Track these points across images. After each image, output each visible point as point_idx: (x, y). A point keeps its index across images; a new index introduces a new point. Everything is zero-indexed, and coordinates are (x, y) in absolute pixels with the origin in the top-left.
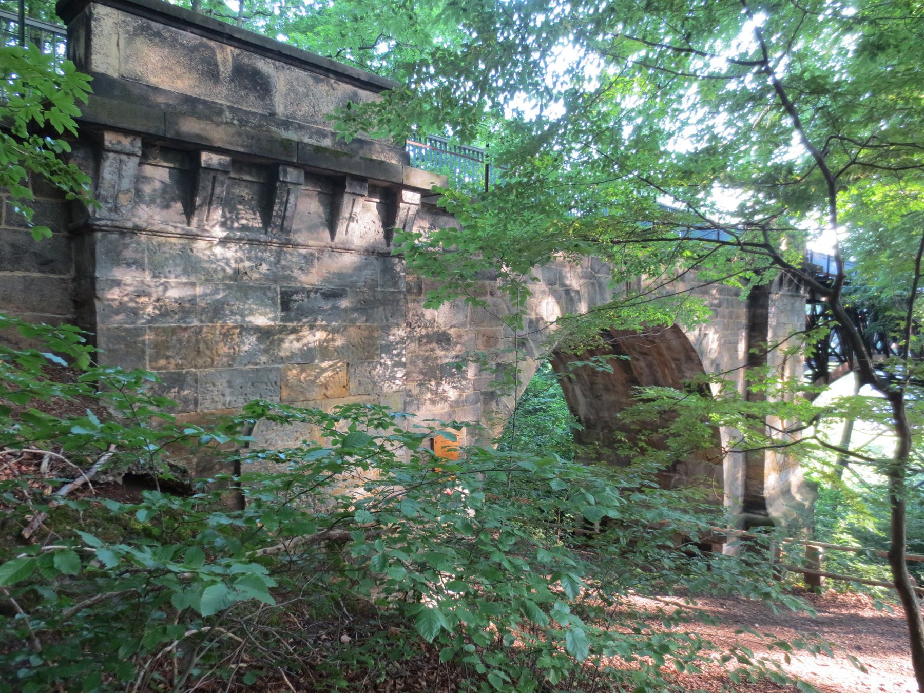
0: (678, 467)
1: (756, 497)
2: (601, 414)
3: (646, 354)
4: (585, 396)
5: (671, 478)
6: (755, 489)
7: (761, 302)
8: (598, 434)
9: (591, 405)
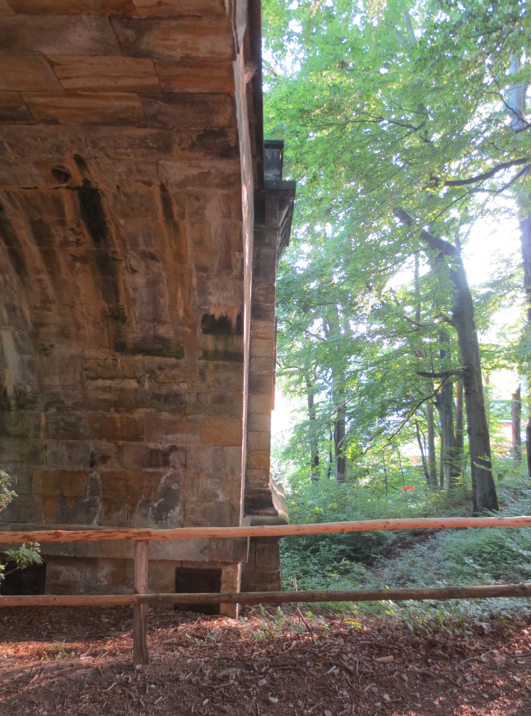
0: (173, 457)
1: (260, 492)
2: (47, 381)
3: (153, 257)
4: (20, 350)
5: (160, 475)
6: (257, 481)
7: (267, 240)
8: (38, 417)
9: (31, 365)
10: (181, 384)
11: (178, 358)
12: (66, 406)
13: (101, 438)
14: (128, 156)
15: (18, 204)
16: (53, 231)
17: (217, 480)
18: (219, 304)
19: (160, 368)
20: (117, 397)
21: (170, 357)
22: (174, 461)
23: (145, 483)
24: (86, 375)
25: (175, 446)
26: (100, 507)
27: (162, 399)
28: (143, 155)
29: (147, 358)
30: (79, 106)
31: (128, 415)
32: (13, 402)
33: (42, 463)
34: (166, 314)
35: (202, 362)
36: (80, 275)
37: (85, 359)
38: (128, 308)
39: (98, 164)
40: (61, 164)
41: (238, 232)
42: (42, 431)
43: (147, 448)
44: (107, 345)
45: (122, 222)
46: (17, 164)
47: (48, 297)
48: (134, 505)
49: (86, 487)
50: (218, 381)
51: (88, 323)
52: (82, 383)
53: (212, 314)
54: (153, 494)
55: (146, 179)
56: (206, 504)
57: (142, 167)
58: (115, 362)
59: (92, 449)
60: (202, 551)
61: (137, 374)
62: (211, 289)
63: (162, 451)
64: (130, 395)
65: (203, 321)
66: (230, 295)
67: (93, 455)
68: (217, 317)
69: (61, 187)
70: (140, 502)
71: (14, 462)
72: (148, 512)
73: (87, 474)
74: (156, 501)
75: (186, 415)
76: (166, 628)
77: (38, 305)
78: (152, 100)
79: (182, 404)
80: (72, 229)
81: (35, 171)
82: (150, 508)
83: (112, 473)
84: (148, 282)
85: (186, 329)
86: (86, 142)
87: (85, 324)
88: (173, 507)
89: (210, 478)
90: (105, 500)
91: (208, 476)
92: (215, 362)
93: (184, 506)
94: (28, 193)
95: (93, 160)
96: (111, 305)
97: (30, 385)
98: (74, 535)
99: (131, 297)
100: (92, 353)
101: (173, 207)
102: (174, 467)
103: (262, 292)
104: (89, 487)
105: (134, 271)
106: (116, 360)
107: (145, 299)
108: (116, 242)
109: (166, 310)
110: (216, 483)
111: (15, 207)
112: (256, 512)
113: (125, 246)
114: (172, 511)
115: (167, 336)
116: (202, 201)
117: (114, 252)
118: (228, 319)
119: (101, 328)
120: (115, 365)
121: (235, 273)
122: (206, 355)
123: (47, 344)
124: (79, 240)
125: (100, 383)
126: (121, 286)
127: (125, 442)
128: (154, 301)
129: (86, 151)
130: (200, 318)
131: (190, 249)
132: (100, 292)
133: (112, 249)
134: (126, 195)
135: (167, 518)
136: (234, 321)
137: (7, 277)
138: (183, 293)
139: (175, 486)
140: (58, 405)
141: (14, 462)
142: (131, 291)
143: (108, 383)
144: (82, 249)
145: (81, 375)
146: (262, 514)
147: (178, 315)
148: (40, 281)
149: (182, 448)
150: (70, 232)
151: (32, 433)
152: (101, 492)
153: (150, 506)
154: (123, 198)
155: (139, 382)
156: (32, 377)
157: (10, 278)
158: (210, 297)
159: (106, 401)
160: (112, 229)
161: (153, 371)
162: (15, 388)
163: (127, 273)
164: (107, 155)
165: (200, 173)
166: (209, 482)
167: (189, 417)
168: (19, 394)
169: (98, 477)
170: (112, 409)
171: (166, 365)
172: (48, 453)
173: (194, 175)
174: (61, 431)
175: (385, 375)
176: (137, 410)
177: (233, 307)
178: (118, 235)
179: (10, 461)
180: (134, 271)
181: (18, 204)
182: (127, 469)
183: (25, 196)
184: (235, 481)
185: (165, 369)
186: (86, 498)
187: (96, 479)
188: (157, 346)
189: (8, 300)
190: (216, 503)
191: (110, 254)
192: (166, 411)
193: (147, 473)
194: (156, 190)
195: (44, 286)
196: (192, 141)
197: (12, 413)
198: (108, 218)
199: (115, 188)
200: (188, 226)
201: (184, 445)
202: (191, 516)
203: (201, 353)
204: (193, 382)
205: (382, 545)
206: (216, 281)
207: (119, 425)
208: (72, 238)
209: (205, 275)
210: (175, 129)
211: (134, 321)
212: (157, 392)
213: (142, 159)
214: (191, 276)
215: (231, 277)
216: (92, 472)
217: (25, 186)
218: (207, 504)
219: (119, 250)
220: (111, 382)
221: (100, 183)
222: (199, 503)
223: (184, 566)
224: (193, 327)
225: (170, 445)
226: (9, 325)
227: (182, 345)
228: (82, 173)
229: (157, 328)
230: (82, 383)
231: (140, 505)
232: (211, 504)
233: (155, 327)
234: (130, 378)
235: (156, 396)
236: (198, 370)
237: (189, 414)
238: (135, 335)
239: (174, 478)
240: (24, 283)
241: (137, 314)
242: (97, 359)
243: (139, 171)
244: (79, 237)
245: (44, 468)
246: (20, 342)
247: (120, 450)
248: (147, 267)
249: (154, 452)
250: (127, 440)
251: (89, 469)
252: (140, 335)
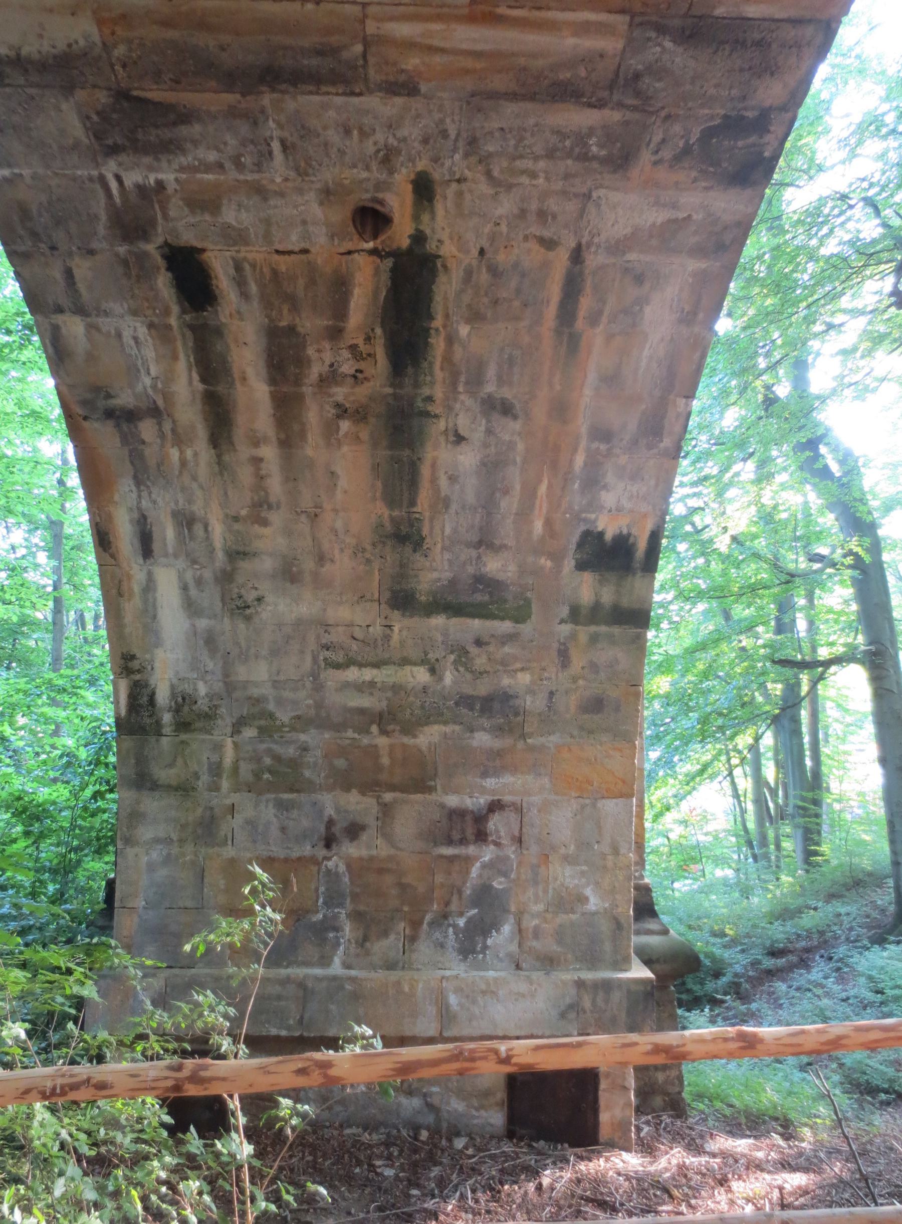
0: (495, 823)
2: (242, 673)
4: (191, 607)
5: (468, 861)
8: (218, 747)
9: (210, 641)
10: (520, 675)
11: (517, 621)
12: (278, 723)
13: (347, 789)
14: (533, 175)
15: (253, 288)
16: (311, 351)
17: (584, 868)
18: (619, 510)
19: (479, 643)
20: (384, 704)
21: (502, 619)
22: (497, 831)
23: (439, 879)
24: (325, 659)
25: (499, 801)
26: (347, 929)
27: (478, 707)
28: (567, 176)
29: (455, 620)
30: (479, 47)
31: (407, 740)
32: (167, 718)
33: (225, 843)
34: (507, 532)
35: (566, 628)
36: (345, 449)
37: (326, 627)
38: (431, 520)
39: (460, 194)
40: (380, 195)
41: (698, 354)
42: (225, 776)
43: (442, 806)
44: (376, 596)
45: (464, 330)
46: (282, 194)
47: (267, 493)
48: (416, 925)
49: (317, 890)
50: (594, 667)
51: (342, 550)
52: (315, 676)
53: (600, 529)
54: (455, 899)
55: (547, 234)
56: (562, 918)
57: (552, 204)
58: (388, 631)
59: (330, 811)
60: (563, 1015)
61: (430, 656)
62: (610, 478)
63: (472, 812)
64: (411, 699)
65: (580, 545)
66: (644, 489)
67: (330, 823)
68: (608, 536)
69: (358, 251)
70: (428, 918)
71: (168, 841)
72: (446, 937)
73: (318, 863)
74: (461, 914)
75: (523, 736)
76: (516, 1182)
77: (244, 512)
78: (653, 34)
79: (517, 714)
80: (353, 348)
81: (317, 211)
82: (451, 930)
83: (371, 859)
84: (484, 464)
85: (542, 561)
86: (456, 140)
87: (337, 552)
88: (495, 925)
89: (570, 863)
90: (357, 916)
91: (567, 860)
92: (593, 628)
93: (519, 923)
94: (284, 264)
95: (454, 185)
96: (396, 513)
97: (206, 682)
98: (794, 1040)
99: (443, 494)
100: (343, 613)
101: (582, 300)
102: (497, 844)
104: (322, 889)
105: (460, 439)
106: (390, 627)
107: (470, 497)
108: (439, 374)
109: (509, 521)
110: (583, 873)
111: (245, 295)
113: (454, 384)
114: (494, 933)
115: (501, 576)
116: (647, 286)
117: (430, 399)
118: (631, 540)
119: (368, 561)
120: (387, 638)
121: (667, 442)
122: (575, 615)
123: (250, 597)
124: (361, 372)
125: (352, 674)
126: (425, 471)
127: (398, 795)
128: (488, 504)
129: (448, 163)
130: (575, 538)
131: (588, 392)
132: (379, 484)
133: (426, 391)
134: (494, 271)
135: (485, 947)
136: (642, 545)
137: (189, 453)
138: (550, 486)
139: (500, 883)
140: (263, 723)
141: (168, 841)
142: (443, 482)
143: (368, 674)
144: (362, 392)
145: (315, 659)
147: (530, 532)
148: (257, 461)
149: (513, 804)
150: (346, 354)
151: (205, 778)
152: (348, 901)
153: (449, 925)
154: (484, 277)
155: (433, 671)
156: (210, 665)
157: (196, 454)
159: (362, 711)
160: (438, 344)
161: (463, 648)
162: (173, 687)
163: (443, 444)
164: (488, 174)
165: (670, 221)
166: (568, 871)
167: (529, 741)
168: (180, 699)
169: (342, 868)
170: (374, 729)
171: (493, 636)
172: (239, 819)
173: (654, 225)
174: (266, 776)
175: (710, 666)
176: (426, 728)
177: (645, 516)
178: (448, 359)
179: (157, 840)
180: (460, 439)
181: (253, 288)
182: (401, 850)
183: (275, 273)
184: (621, 869)
185: (487, 644)
186: (317, 912)
187: (337, 874)
188: (479, 598)
189: (181, 502)
190: (583, 914)
191: (419, 404)
192: (484, 730)
193: (442, 857)
194: (561, 258)
195: (263, 472)
196: (687, 142)
197: (165, 741)
198: (438, 323)
199: (475, 252)
200: (599, 341)
201: (516, 799)
202: (534, 943)
203: (565, 611)
204: (544, 669)
205: (724, 975)
206: (623, 459)
207: (385, 761)
208: (347, 368)
209: (603, 447)
210: (663, 114)
211: (439, 546)
212: (468, 690)
213: (559, 185)
214: (575, 450)
215: (655, 451)
216: (329, 859)
217: (281, 248)
218: (565, 916)
219: (439, 393)
220: (375, 671)
221: (447, 242)
222: (549, 916)
224: (557, 557)
225: (490, 798)
226: (176, 556)
227: (529, 594)
228: (416, 218)
229: (484, 559)
230: (315, 676)
231: (431, 924)
232: (573, 917)
233: (479, 557)
234: (415, 664)
235: (466, 701)
236: (555, 645)
237: (531, 735)
238: (435, 575)
239: (498, 867)
240: (221, 466)
241: (448, 531)
242: (351, 625)
243: (542, 215)
244: (362, 365)
245: (229, 852)
246: (193, 592)
247: (386, 810)
248: (489, 432)
249: (457, 815)
250: (402, 791)
251: (322, 852)
252: (448, 574)
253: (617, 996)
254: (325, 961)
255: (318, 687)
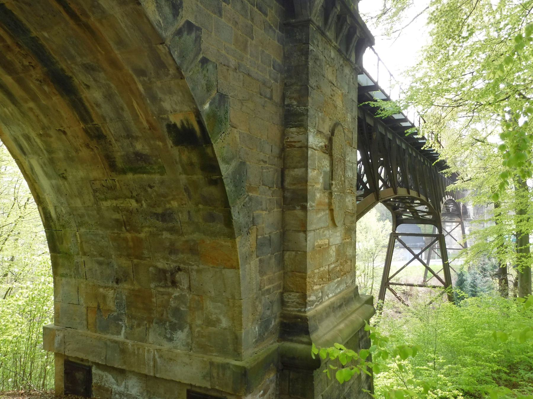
1: (297, 317)
41: (145, 20)
53: (173, 123)
62: (160, 95)
68: (179, 125)
85: (157, 143)
93: (191, 328)
103: (295, 95)
112: (290, 338)
130: (165, 130)
131: (117, 52)
136: (197, 128)
139: (183, 308)
146: (296, 342)
155: (137, 201)
158: (162, 103)
211: (113, 139)
215: (170, 76)
223: (194, 389)
241: (112, 132)
253: (228, 373)
254: (119, 333)
255: (99, 210)
